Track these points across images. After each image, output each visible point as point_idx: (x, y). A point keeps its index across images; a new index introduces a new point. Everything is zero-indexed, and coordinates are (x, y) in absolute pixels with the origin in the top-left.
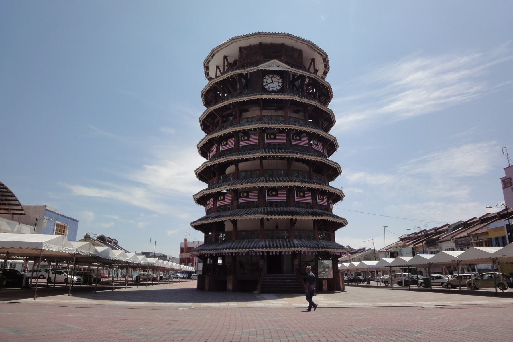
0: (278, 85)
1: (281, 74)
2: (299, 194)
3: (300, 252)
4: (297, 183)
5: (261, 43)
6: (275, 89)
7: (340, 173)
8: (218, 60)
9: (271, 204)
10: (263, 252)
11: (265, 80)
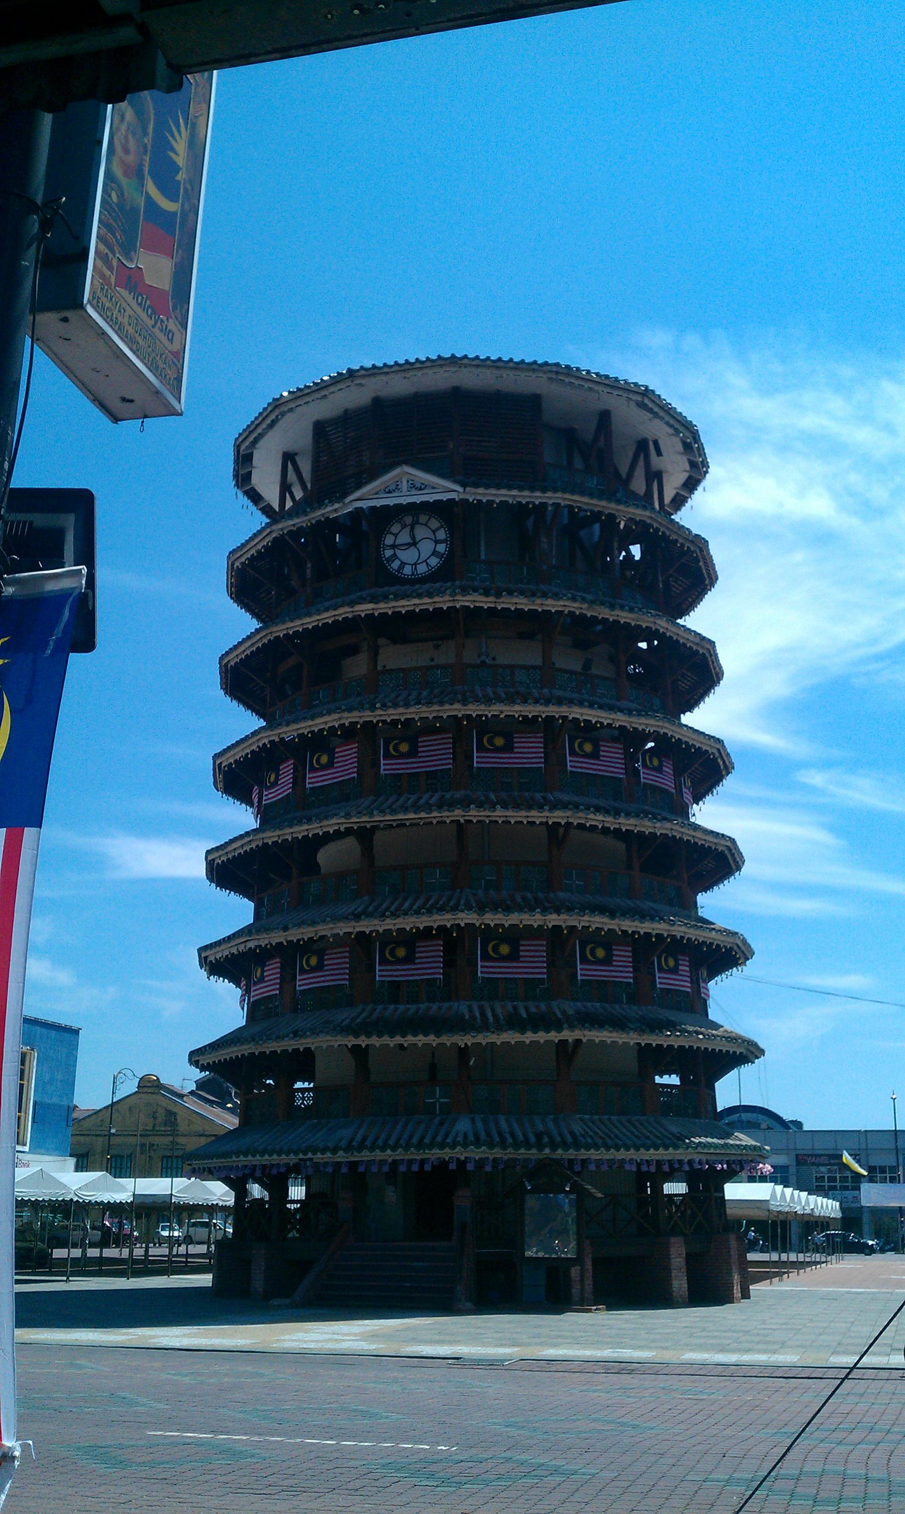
0: (435, 553)
1: (441, 510)
2: (593, 953)
3: (462, 1164)
4: (461, 915)
5: (377, 401)
6: (422, 569)
7: (739, 868)
9: (395, 991)
10: (338, 1164)
11: (389, 540)
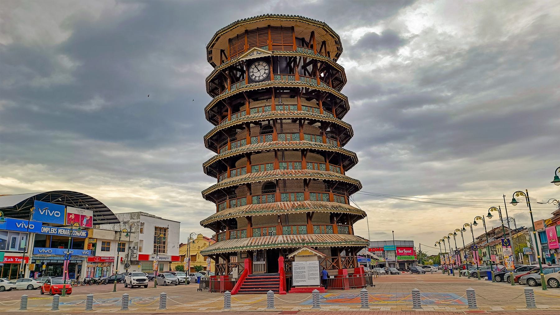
1: (266, 60)
6: (261, 78)
8: (223, 44)
